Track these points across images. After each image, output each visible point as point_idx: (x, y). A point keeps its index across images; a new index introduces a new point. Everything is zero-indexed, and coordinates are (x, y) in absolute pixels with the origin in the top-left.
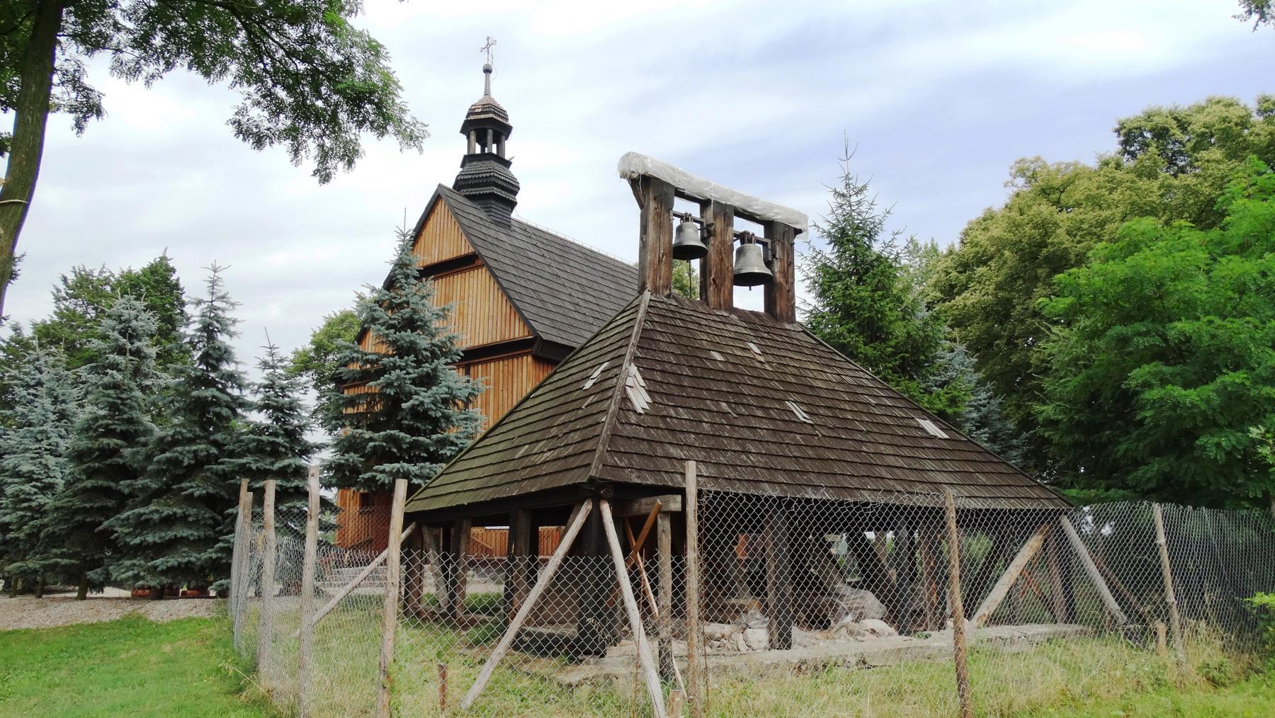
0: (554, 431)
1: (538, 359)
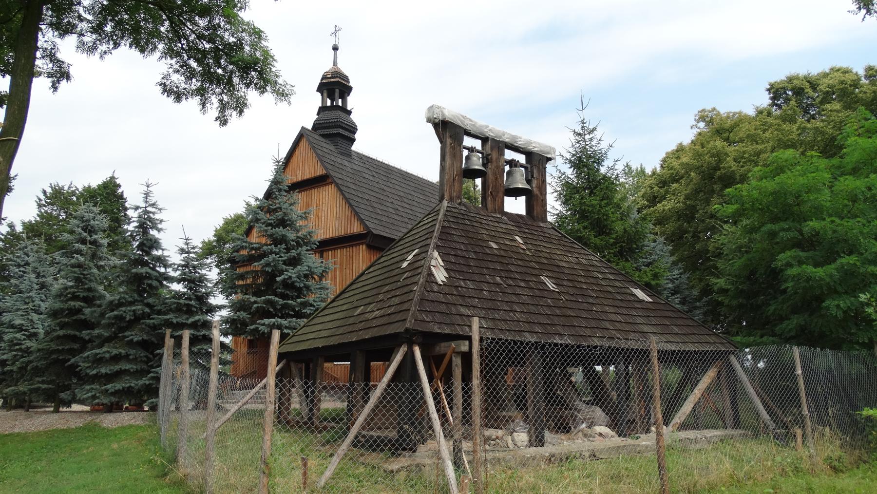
0: (381, 297)
1: (370, 247)
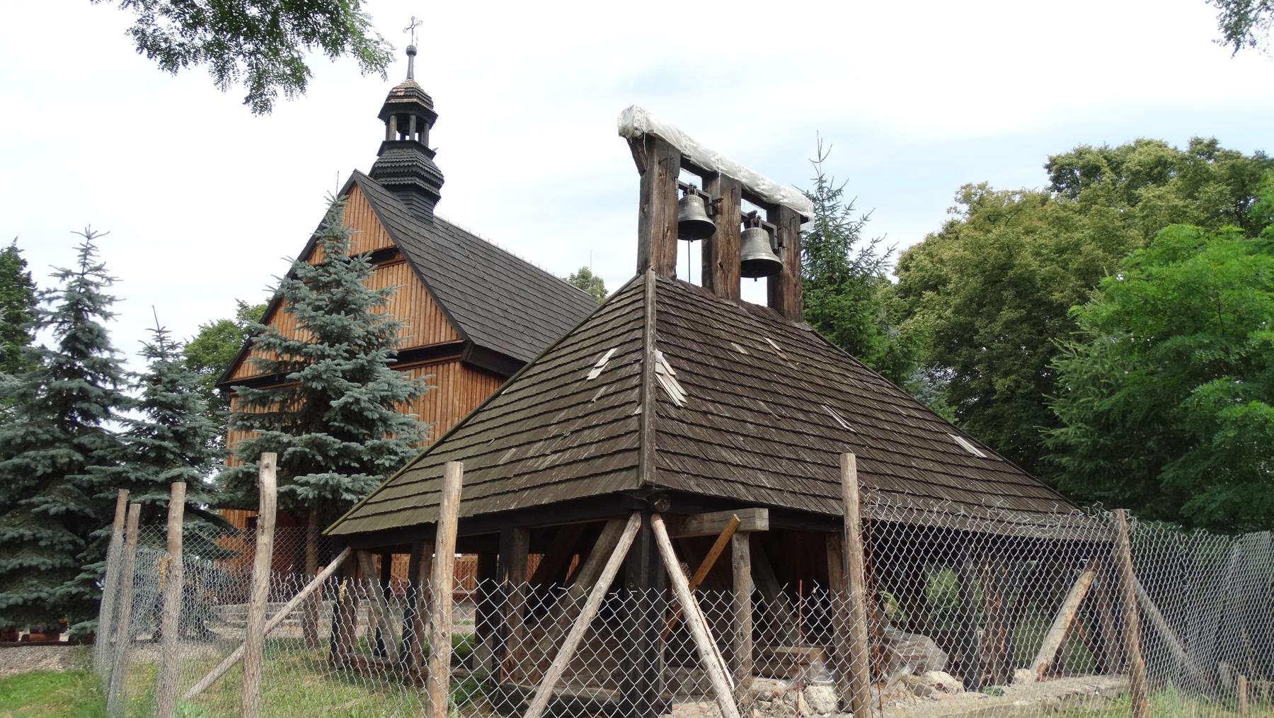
0: (554, 430)
1: (467, 366)
